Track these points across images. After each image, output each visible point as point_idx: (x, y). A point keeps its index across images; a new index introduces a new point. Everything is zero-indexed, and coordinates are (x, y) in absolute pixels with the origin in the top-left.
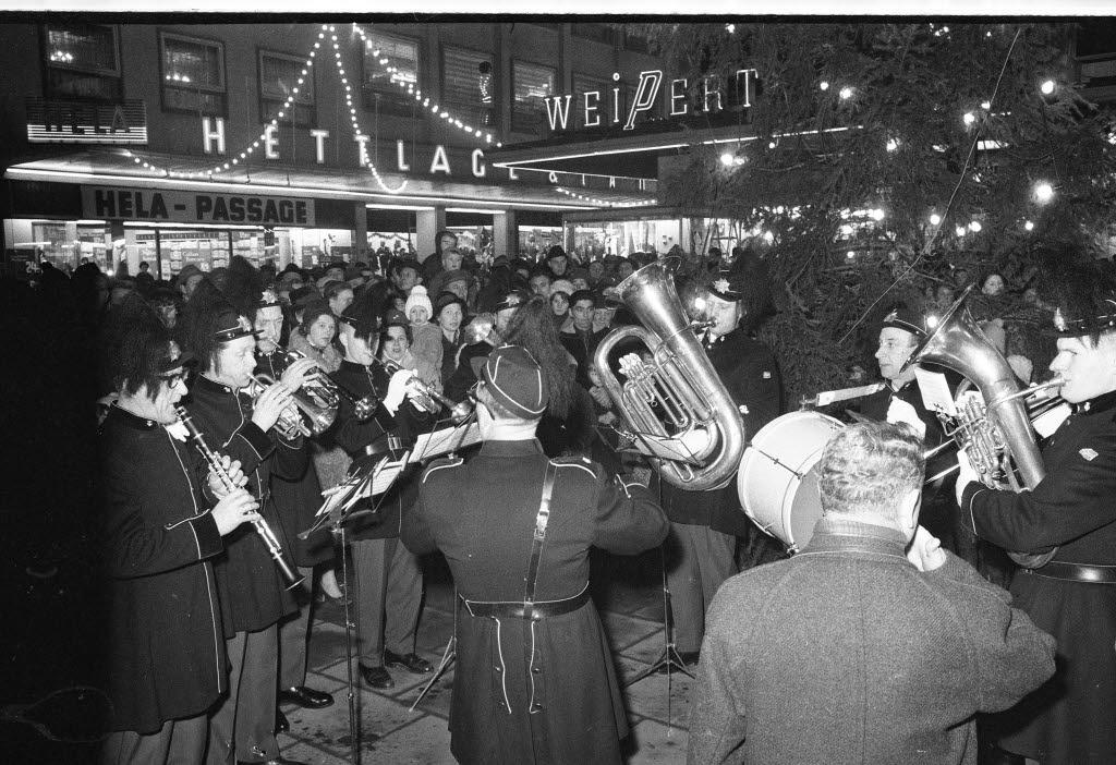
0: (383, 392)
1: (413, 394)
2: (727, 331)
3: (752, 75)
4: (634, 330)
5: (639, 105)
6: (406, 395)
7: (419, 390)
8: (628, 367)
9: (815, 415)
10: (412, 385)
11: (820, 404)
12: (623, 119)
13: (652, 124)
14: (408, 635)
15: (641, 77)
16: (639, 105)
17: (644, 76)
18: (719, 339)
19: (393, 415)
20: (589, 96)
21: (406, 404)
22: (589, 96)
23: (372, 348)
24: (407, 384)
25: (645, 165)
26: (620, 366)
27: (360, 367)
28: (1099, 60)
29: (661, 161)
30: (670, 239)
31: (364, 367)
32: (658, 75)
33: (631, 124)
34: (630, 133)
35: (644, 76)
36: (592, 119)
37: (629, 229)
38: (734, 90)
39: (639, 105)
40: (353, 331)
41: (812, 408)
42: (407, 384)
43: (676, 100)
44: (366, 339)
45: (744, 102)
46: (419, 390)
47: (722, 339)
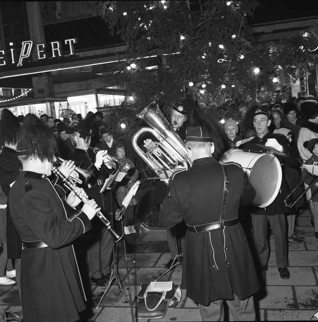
0: (94, 160)
1: (106, 161)
2: (180, 126)
3: (72, 41)
4: (144, 130)
5: (23, 55)
6: (103, 161)
7: (108, 159)
8: (148, 144)
9: (237, 150)
10: (106, 157)
11: (237, 146)
12: (17, 60)
13: (29, 63)
14: (107, 265)
15: (23, 44)
16: (23, 55)
17: (24, 43)
18: (177, 130)
19: (99, 170)
20: (67, 41)
21: (103, 165)
22: (67, 41)
23: (87, 142)
24: (103, 156)
25: (26, 82)
26: (144, 144)
27: (82, 151)
28: (299, 20)
29: (34, 79)
30: (42, 112)
31: (85, 151)
32: (30, 43)
33: (20, 63)
34: (20, 68)
35: (24, 43)
36: (42, 56)
37: (21, 110)
38: (65, 48)
39: (23, 55)
40: (79, 135)
41: (235, 148)
42: (103, 156)
43: (40, 53)
44: (85, 139)
45: (70, 53)
46: (108, 159)
47: (179, 130)
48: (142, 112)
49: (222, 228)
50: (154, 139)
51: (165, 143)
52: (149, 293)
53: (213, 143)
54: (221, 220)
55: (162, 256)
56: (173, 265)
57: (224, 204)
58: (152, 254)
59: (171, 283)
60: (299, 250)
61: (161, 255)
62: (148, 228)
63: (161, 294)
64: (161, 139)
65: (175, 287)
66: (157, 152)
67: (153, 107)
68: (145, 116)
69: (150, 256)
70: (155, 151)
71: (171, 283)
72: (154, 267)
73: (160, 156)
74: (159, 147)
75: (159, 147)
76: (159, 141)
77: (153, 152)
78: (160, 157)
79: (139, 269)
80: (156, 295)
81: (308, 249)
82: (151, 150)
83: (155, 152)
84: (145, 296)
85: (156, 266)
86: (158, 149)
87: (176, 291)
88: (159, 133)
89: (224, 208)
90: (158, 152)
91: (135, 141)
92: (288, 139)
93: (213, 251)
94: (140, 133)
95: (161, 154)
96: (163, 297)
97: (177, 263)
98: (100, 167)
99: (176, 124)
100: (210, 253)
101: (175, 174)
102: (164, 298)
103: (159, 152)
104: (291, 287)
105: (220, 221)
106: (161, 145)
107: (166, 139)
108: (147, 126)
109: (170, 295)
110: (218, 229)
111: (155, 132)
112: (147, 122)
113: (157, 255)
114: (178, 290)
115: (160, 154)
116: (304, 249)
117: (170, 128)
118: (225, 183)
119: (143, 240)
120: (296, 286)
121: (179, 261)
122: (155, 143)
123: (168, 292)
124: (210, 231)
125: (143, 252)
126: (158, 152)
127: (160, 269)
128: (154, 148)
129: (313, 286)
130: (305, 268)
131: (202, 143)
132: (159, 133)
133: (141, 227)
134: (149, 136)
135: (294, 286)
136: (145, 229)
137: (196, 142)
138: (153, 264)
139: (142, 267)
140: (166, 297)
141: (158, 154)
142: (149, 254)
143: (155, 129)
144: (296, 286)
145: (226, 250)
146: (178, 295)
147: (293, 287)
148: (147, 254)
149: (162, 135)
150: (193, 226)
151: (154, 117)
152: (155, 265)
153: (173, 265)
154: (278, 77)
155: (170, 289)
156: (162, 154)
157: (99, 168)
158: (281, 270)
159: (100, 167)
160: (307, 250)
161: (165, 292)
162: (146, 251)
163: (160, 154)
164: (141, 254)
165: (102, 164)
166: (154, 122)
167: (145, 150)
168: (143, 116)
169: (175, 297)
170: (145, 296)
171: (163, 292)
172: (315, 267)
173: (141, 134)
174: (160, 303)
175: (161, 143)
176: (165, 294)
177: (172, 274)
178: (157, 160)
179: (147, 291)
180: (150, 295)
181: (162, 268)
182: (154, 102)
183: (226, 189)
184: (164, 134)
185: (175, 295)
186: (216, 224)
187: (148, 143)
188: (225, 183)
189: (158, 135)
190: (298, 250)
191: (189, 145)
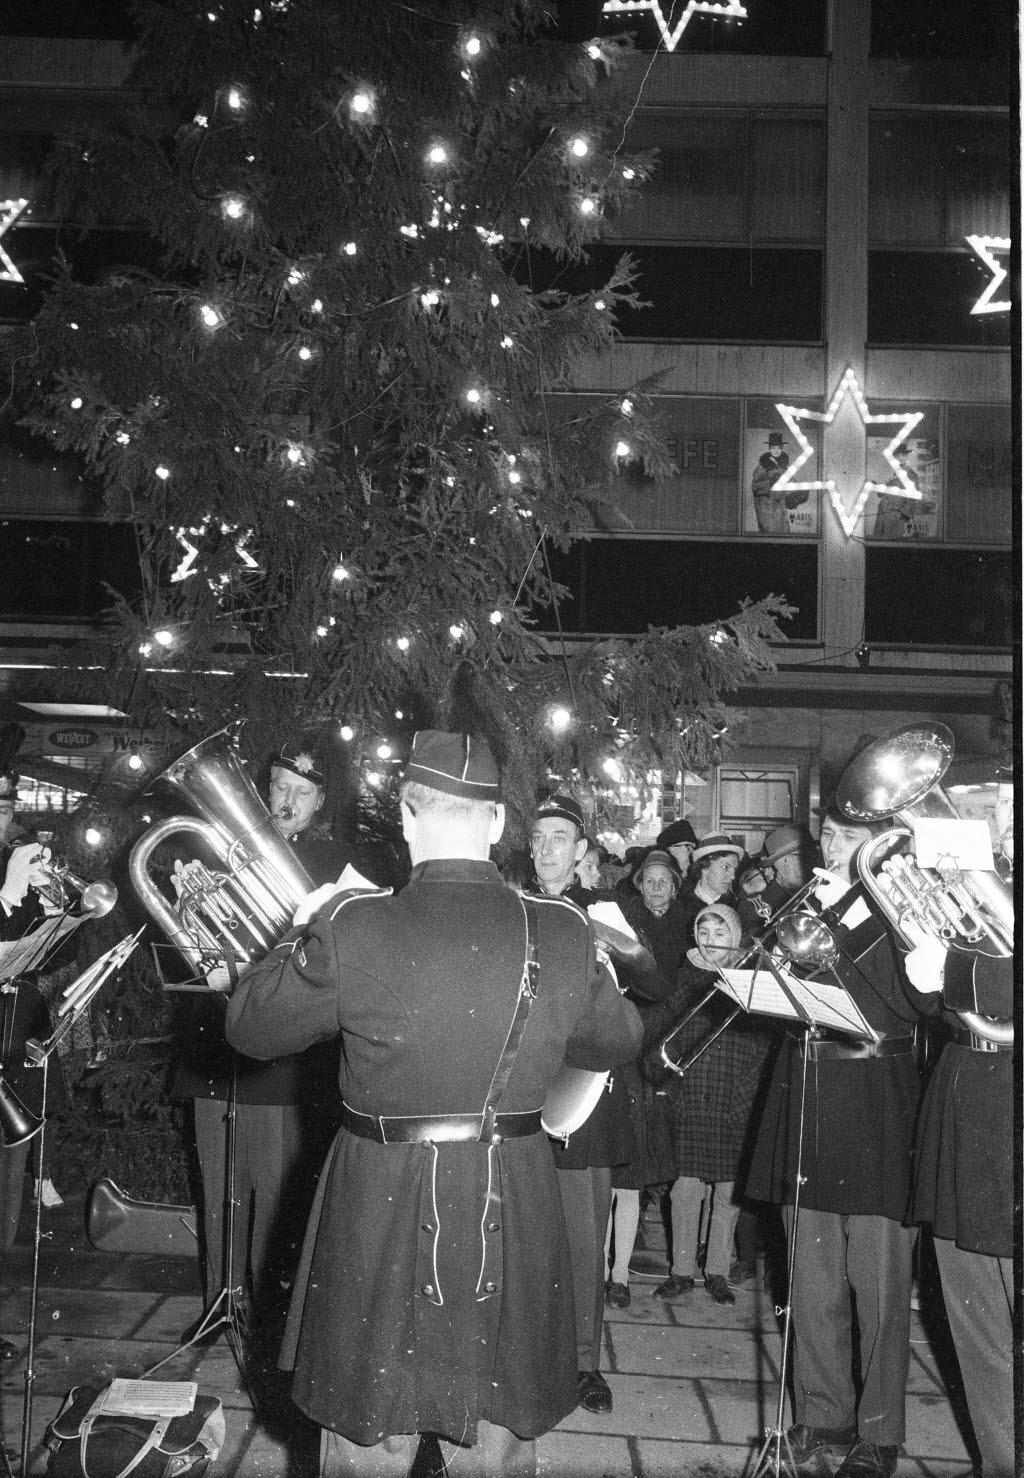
4: (176, 823)
19: (9, 913)
47: (295, 839)
48: (180, 763)
49: (485, 1139)
50: (214, 863)
51: (246, 877)
52: (101, 1419)
53: (501, 808)
54: (487, 1110)
55: (161, 1304)
56: (203, 1331)
57: (512, 1046)
58: (126, 1295)
59: (193, 1387)
60: (651, 1321)
61: (160, 1302)
62: (124, 1201)
63: (147, 1425)
64: (235, 863)
65: (204, 1404)
66: (218, 905)
67: (216, 751)
68: (186, 777)
69: (117, 1302)
70: (210, 902)
71: (193, 1387)
72: (130, 1336)
73: (224, 919)
74: (228, 888)
75: (228, 888)
76: (226, 869)
77: (203, 904)
78: (226, 924)
79: (71, 1340)
80: (128, 1428)
81: (680, 1320)
82: (196, 897)
83: (210, 907)
84: (85, 1430)
85: (137, 1336)
86: (223, 897)
87: (207, 1423)
88: (231, 840)
89: (504, 1067)
90: (221, 908)
91: (142, 861)
92: (219, 1342)
93: (434, 1225)
94: (162, 834)
95: (230, 913)
96: (155, 1441)
97: (224, 1319)
98: (20, 904)
99: (289, 816)
100: (421, 1232)
101: (347, 901)
102: (159, 1443)
103: (225, 907)
104: (624, 1442)
105: (484, 1113)
106: (233, 883)
107: (252, 864)
108: (192, 812)
109: (184, 1431)
110: (471, 1140)
111: (214, 836)
112: (194, 798)
113: (148, 1299)
114: (216, 1419)
115: (227, 916)
116: (665, 1321)
117: (268, 826)
118: (526, 966)
119: (98, 1244)
120: (643, 1438)
121: (233, 1313)
122: (213, 874)
123: (175, 1420)
124: (440, 1145)
125: (94, 1286)
126: (221, 908)
127: (147, 1346)
128: (209, 892)
129: (704, 1443)
130: (673, 1381)
131: (459, 800)
132: (231, 840)
133: (102, 1192)
134: (186, 846)
135: (635, 1438)
136: (115, 1201)
137: (440, 794)
138: (129, 1327)
139: (82, 1336)
140: (165, 1440)
141: (219, 912)
142: (117, 1295)
143: (217, 825)
144: (643, 1438)
145: (487, 1229)
146: (211, 1435)
147: (632, 1442)
148: (108, 1294)
149: (239, 849)
150: (377, 1115)
151: (215, 780)
152: (135, 1331)
153: (203, 1331)
154: (619, 758)
155: (185, 1408)
156: (236, 916)
157: (14, 908)
158: (585, 1380)
159: (20, 904)
160: (674, 1322)
161: (166, 1419)
162: (108, 1282)
163: (227, 916)
164: (88, 1292)
165: (26, 894)
166: (220, 800)
167: (168, 891)
168: (181, 776)
169: (200, 1444)
170: (85, 1430)
171: (154, 1419)
172: (705, 1383)
173: (151, 849)
174: (140, 1460)
175: (235, 877)
176: (164, 1427)
177: (196, 1366)
178: (215, 935)
179: (95, 1411)
180: (105, 1426)
181: (157, 1344)
182: (225, 731)
183: (527, 989)
184: (248, 844)
185: (202, 1436)
186: (466, 1120)
187: (184, 873)
188: (526, 966)
189: (226, 847)
190: (644, 1321)
191: (412, 795)
